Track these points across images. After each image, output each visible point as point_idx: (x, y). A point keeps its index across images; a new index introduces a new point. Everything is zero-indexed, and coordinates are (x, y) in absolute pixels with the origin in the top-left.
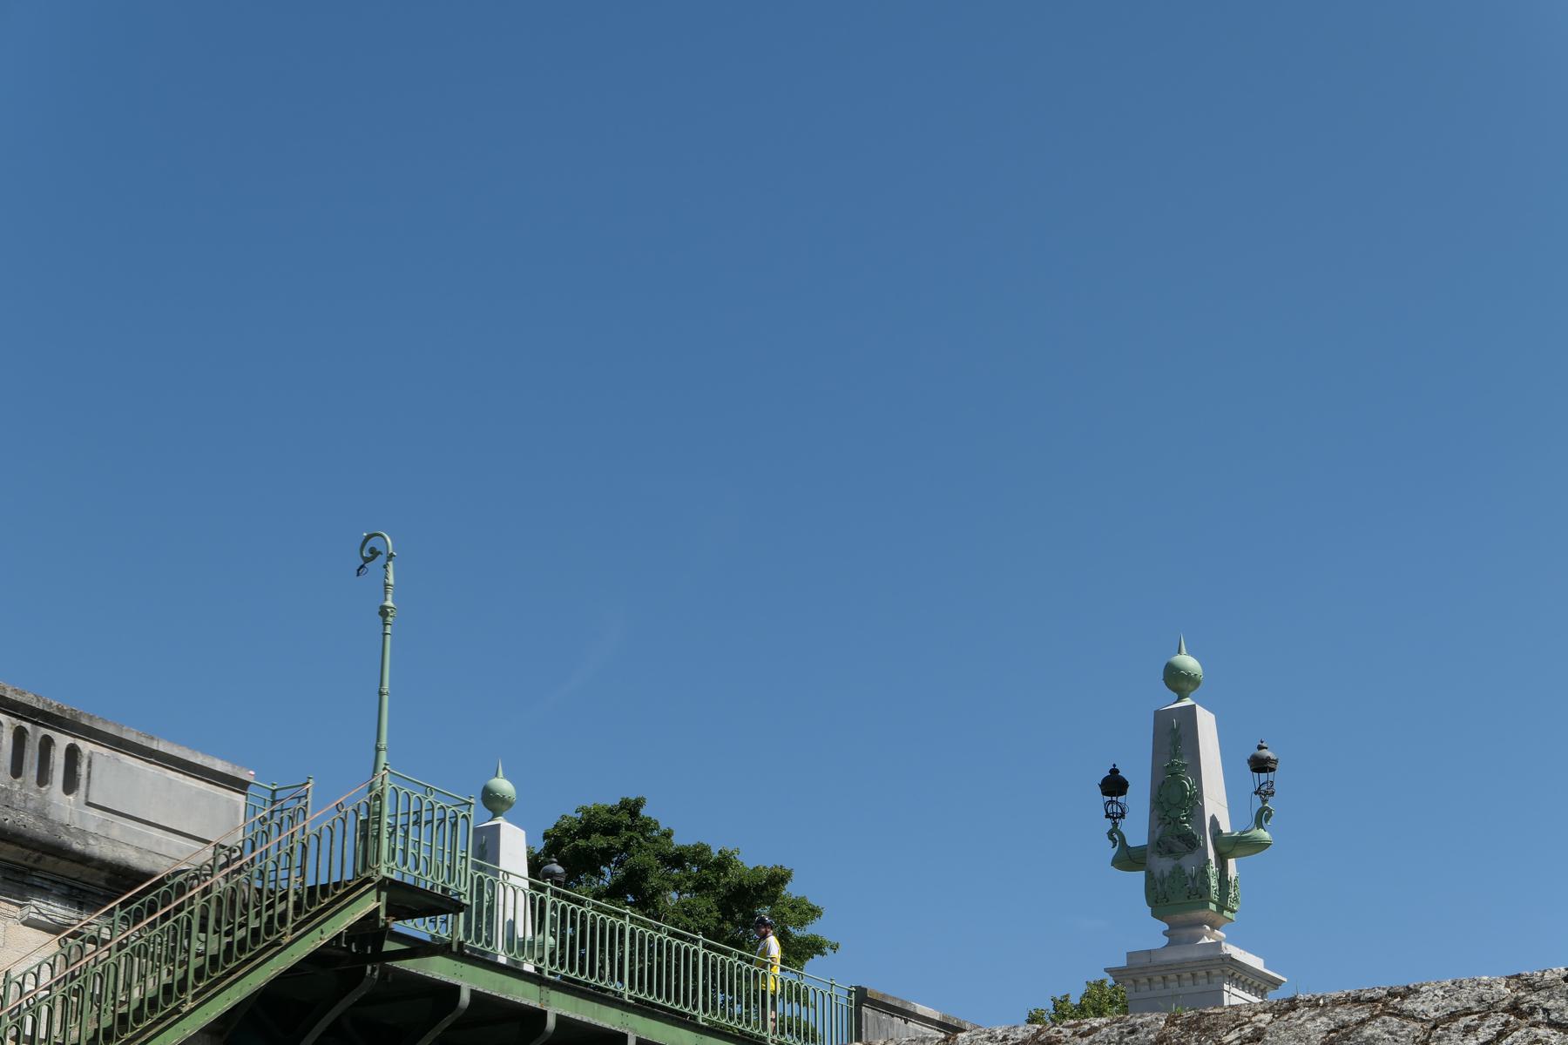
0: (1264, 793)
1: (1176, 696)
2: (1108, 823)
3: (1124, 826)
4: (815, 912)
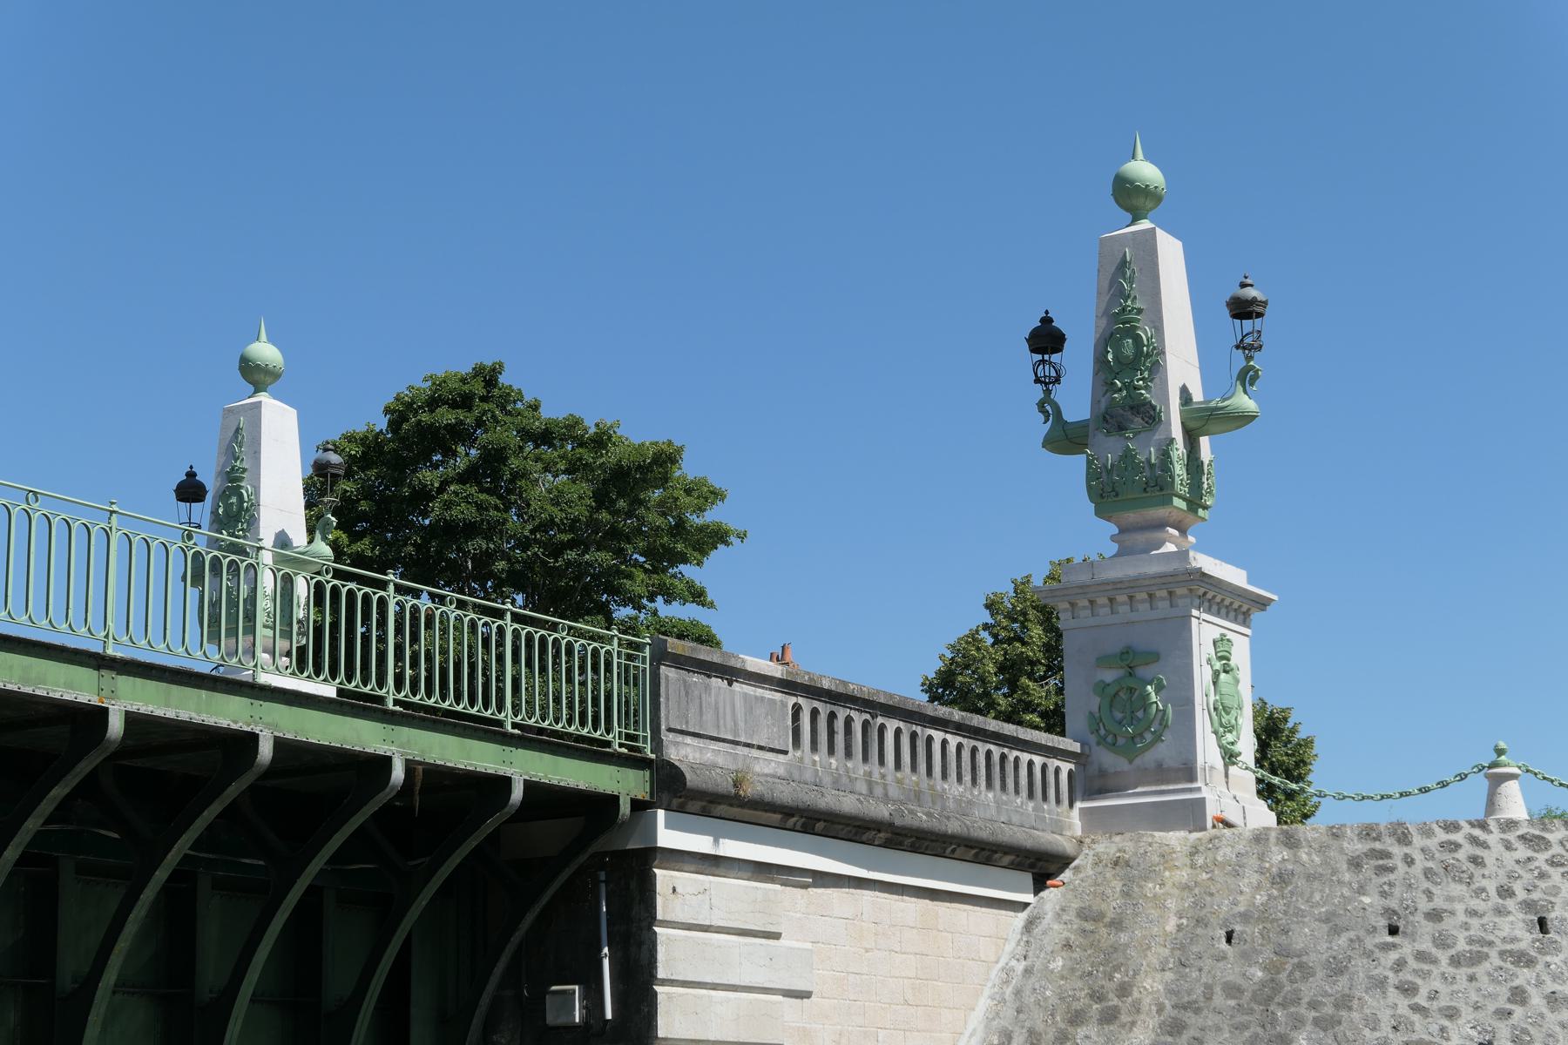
0: (1247, 347)
1: (1129, 217)
2: (1038, 392)
3: (1059, 393)
4: (716, 495)
